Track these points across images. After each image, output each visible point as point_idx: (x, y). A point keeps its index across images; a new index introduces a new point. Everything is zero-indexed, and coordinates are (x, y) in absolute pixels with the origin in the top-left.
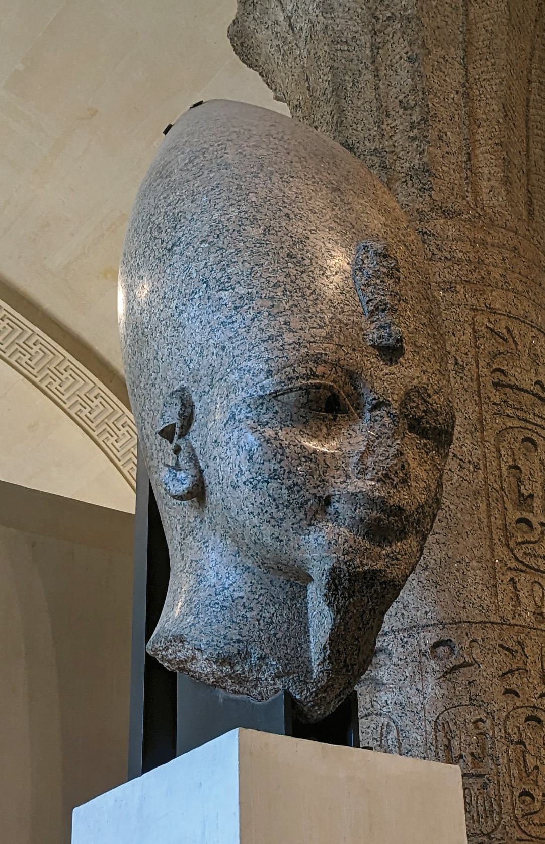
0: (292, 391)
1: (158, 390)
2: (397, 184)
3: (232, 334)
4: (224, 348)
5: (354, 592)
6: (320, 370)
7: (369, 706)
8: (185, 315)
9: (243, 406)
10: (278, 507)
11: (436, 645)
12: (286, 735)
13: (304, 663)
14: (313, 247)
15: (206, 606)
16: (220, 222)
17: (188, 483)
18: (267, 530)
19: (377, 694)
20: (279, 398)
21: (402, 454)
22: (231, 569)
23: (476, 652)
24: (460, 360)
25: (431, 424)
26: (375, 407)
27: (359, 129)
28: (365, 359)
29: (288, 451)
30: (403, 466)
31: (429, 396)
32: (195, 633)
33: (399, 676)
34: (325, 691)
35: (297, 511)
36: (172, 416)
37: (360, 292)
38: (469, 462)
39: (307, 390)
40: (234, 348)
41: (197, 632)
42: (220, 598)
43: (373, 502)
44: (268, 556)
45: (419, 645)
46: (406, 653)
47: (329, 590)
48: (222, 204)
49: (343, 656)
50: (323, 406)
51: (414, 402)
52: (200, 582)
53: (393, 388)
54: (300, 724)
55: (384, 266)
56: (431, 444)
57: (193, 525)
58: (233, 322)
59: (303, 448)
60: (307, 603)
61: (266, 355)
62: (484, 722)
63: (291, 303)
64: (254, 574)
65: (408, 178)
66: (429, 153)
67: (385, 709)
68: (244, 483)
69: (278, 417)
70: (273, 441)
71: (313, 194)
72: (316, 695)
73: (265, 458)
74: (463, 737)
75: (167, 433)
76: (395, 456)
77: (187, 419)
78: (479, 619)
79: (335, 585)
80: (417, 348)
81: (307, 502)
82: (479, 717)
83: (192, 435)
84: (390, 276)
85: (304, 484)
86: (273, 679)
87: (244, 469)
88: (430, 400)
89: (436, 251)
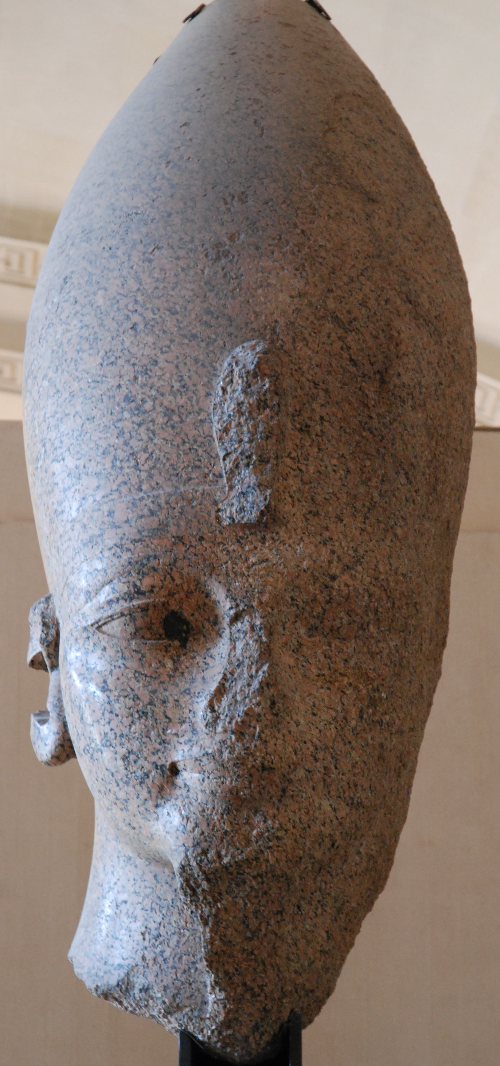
0: (113, 619)
5: (220, 894)
13: (199, 990)
14: (160, 378)
20: (104, 628)
35: (138, 787)
49: (237, 979)
50: (161, 631)
64: (136, 866)
72: (220, 1033)
76: (261, 690)
81: (147, 775)
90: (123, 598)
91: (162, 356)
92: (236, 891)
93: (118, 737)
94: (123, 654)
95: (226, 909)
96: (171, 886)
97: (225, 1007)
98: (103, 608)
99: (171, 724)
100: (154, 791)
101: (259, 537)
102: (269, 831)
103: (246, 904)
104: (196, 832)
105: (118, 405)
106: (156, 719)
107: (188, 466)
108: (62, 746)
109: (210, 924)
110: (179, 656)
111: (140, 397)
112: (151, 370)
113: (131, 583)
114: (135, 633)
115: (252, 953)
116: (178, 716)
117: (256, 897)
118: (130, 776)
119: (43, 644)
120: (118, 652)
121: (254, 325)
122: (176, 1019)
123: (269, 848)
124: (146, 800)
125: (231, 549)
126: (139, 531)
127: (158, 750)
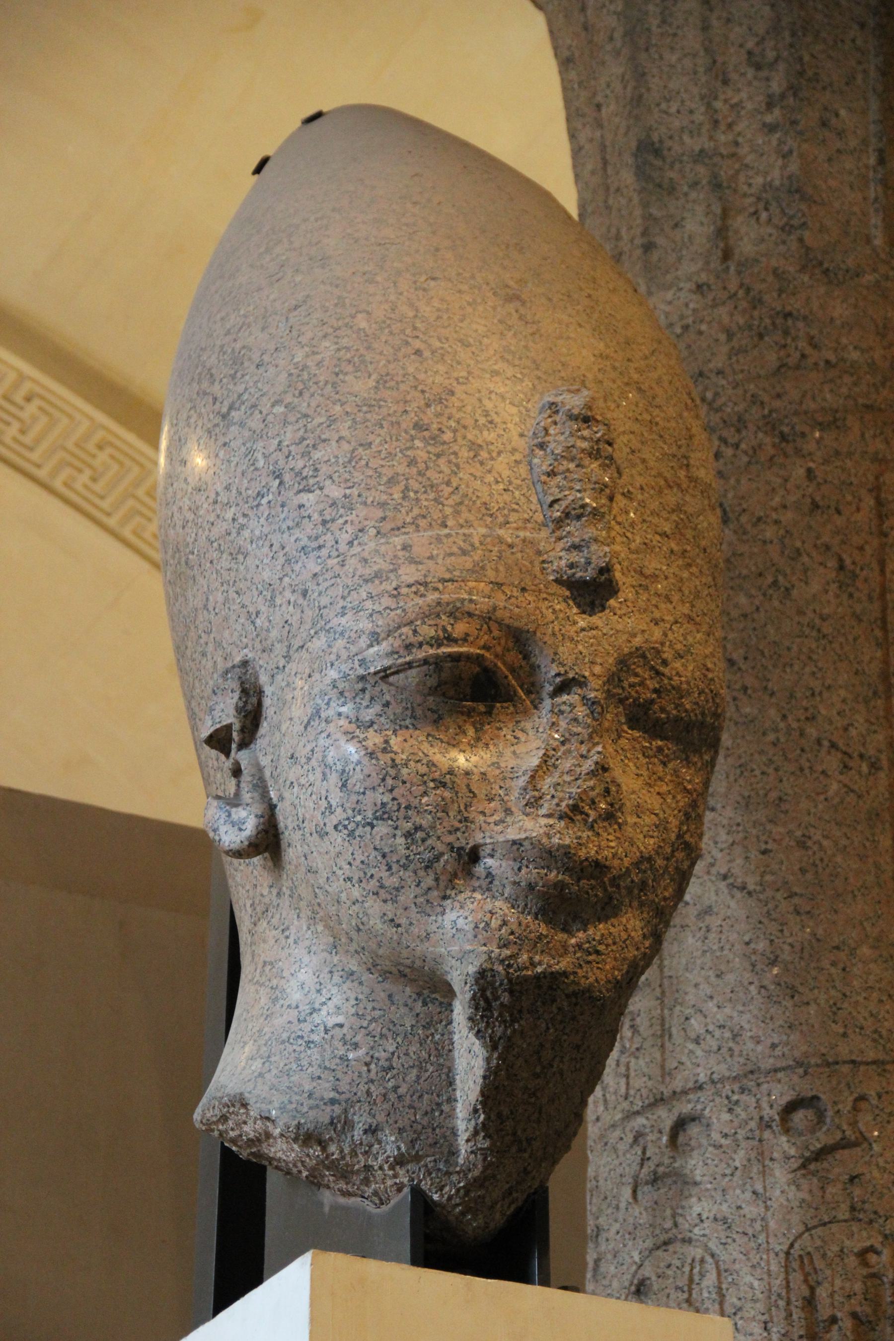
1: (210, 664)
2: (740, 219)
3: (317, 569)
4: (305, 594)
5: (520, 1012)
6: (460, 629)
7: (668, 1224)
8: (246, 533)
9: (333, 694)
10: (390, 868)
11: (790, 1108)
12: (416, 1261)
14: (460, 409)
15: (283, 1042)
16: (305, 367)
17: (250, 826)
18: (374, 907)
19: (684, 1203)
20: (391, 679)
21: (605, 769)
22: (324, 975)
23: (865, 1120)
24: (848, 561)
25: (668, 713)
26: (564, 687)
27: (673, 110)
28: (544, 605)
29: (405, 771)
30: (607, 791)
31: (665, 663)
32: (262, 1090)
33: (723, 1168)
34: (481, 1186)
35: (422, 873)
36: (226, 711)
37: (539, 487)
38: (861, 756)
39: (436, 663)
40: (320, 594)
41: (266, 1088)
42: (307, 1027)
43: (550, 856)
44: (381, 952)
45: (758, 1107)
46: (736, 1124)
47: (477, 1008)
48: (309, 335)
49: (509, 1125)
50: (468, 691)
51: (636, 675)
52: (275, 1001)
53: (595, 653)
54: (440, 1244)
55: (584, 438)
56: (670, 747)
57: (266, 900)
58: (320, 547)
59: (431, 764)
60: (451, 1033)
61: (369, 605)
62: (878, 1253)
63: (416, 511)
64: (361, 983)
65: (761, 206)
66: (801, 156)
67: (696, 1230)
68: (336, 827)
69: (390, 711)
70: (380, 755)
71: (469, 310)
72: (467, 1193)
73: (368, 784)
74: (838, 1282)
75: (219, 741)
76: (592, 774)
77: (252, 716)
78: (871, 1055)
79: (487, 1000)
80: (646, 579)
81: (437, 858)
82: (868, 1244)
83: (261, 743)
84: (594, 454)
85: (433, 827)
86: (392, 1168)
87: (334, 804)
88: (666, 671)
89: (809, 350)
90: (427, 643)
91: (459, 387)
92: (541, 1010)
93: (402, 809)
94: (413, 711)
95: (522, 1032)
96: (411, 1009)
97: (485, 1159)
98: (397, 653)
99: (475, 800)
100: (444, 878)
101: (588, 600)
102: (589, 942)
103: (548, 1028)
104: (503, 931)
105: (406, 432)
106: (457, 793)
107: (504, 508)
108: (266, 832)
109: (500, 1048)
110: (482, 724)
111: (435, 426)
112: (447, 400)
113: (440, 627)
114: (436, 688)
115: (534, 1094)
116: (484, 792)
117: (561, 1022)
118: (412, 857)
119: (240, 713)
120: (407, 708)
121: (563, 374)
122: (408, 1171)
123: (589, 962)
124: (429, 889)
125: (558, 607)
126: (448, 570)
127: (458, 829)
